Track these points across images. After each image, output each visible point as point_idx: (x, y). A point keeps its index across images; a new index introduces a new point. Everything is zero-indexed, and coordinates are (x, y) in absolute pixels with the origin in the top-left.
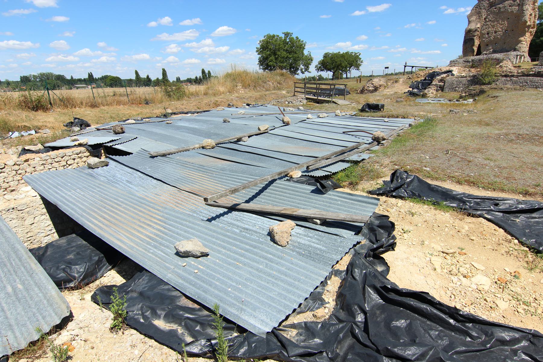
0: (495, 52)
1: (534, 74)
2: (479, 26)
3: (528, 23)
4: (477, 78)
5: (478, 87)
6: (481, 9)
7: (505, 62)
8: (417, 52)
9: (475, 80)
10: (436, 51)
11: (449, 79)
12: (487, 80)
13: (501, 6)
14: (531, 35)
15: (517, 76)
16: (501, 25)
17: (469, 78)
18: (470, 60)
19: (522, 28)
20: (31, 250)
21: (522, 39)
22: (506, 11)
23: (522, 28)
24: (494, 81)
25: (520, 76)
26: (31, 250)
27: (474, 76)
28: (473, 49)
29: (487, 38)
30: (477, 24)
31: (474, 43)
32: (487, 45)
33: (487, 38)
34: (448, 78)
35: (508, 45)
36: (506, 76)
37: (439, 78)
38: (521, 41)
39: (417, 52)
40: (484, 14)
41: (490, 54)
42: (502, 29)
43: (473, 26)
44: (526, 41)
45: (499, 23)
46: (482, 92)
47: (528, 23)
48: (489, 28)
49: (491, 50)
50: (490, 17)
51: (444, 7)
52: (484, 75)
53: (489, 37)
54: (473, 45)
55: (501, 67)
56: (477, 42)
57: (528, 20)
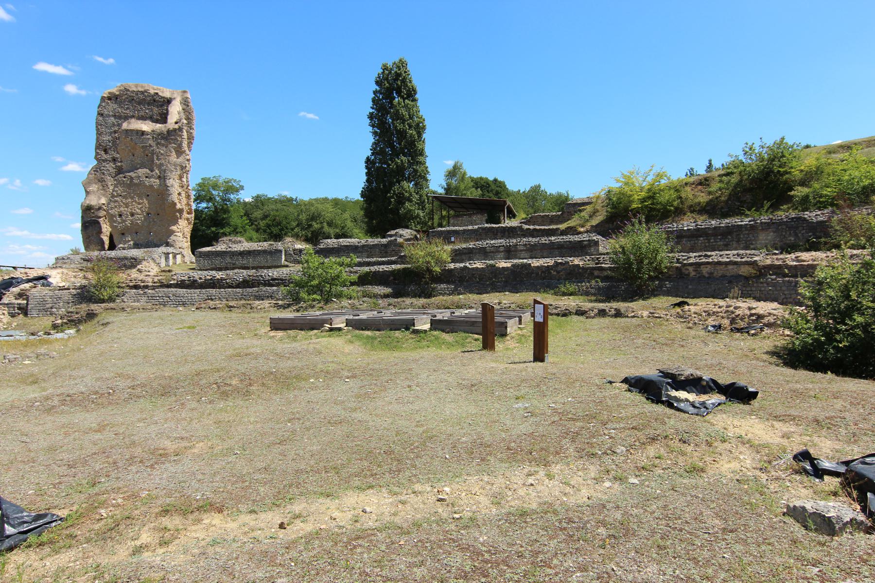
0: (137, 246)
1: (177, 284)
2: (103, 201)
3: (178, 206)
4: (88, 292)
5: (84, 308)
6: (104, 174)
7: (144, 263)
8: (19, 233)
9: (85, 295)
10: (62, 236)
11: (38, 292)
12: (105, 294)
13: (132, 174)
14: (189, 223)
15: (154, 288)
16: (139, 204)
17: (74, 292)
18: (95, 258)
19: (172, 214)
20: (773, 353)
21: (174, 228)
22: (141, 184)
23: (172, 214)
24: (118, 296)
25: (158, 287)
26: (773, 353)
27: (82, 287)
28: (102, 239)
29: (119, 223)
30: (100, 198)
31: (100, 228)
32: (123, 234)
33: (119, 223)
34: (34, 290)
35: (154, 236)
36: (136, 287)
37: (15, 290)
38: (174, 232)
39: (19, 233)
40: (110, 181)
41: (130, 248)
42: (142, 212)
43: (93, 201)
44: (182, 231)
45: (135, 201)
46: (91, 316)
47: (178, 206)
48: (120, 206)
49: (132, 243)
50: (119, 190)
51: (59, 159)
52: (99, 286)
53: (124, 221)
54: (100, 232)
55: (140, 271)
56: (106, 229)
57: (177, 201)
